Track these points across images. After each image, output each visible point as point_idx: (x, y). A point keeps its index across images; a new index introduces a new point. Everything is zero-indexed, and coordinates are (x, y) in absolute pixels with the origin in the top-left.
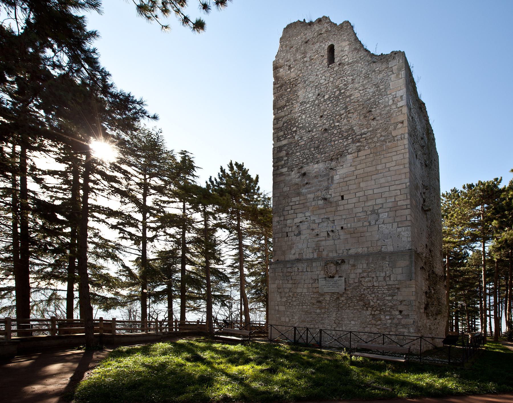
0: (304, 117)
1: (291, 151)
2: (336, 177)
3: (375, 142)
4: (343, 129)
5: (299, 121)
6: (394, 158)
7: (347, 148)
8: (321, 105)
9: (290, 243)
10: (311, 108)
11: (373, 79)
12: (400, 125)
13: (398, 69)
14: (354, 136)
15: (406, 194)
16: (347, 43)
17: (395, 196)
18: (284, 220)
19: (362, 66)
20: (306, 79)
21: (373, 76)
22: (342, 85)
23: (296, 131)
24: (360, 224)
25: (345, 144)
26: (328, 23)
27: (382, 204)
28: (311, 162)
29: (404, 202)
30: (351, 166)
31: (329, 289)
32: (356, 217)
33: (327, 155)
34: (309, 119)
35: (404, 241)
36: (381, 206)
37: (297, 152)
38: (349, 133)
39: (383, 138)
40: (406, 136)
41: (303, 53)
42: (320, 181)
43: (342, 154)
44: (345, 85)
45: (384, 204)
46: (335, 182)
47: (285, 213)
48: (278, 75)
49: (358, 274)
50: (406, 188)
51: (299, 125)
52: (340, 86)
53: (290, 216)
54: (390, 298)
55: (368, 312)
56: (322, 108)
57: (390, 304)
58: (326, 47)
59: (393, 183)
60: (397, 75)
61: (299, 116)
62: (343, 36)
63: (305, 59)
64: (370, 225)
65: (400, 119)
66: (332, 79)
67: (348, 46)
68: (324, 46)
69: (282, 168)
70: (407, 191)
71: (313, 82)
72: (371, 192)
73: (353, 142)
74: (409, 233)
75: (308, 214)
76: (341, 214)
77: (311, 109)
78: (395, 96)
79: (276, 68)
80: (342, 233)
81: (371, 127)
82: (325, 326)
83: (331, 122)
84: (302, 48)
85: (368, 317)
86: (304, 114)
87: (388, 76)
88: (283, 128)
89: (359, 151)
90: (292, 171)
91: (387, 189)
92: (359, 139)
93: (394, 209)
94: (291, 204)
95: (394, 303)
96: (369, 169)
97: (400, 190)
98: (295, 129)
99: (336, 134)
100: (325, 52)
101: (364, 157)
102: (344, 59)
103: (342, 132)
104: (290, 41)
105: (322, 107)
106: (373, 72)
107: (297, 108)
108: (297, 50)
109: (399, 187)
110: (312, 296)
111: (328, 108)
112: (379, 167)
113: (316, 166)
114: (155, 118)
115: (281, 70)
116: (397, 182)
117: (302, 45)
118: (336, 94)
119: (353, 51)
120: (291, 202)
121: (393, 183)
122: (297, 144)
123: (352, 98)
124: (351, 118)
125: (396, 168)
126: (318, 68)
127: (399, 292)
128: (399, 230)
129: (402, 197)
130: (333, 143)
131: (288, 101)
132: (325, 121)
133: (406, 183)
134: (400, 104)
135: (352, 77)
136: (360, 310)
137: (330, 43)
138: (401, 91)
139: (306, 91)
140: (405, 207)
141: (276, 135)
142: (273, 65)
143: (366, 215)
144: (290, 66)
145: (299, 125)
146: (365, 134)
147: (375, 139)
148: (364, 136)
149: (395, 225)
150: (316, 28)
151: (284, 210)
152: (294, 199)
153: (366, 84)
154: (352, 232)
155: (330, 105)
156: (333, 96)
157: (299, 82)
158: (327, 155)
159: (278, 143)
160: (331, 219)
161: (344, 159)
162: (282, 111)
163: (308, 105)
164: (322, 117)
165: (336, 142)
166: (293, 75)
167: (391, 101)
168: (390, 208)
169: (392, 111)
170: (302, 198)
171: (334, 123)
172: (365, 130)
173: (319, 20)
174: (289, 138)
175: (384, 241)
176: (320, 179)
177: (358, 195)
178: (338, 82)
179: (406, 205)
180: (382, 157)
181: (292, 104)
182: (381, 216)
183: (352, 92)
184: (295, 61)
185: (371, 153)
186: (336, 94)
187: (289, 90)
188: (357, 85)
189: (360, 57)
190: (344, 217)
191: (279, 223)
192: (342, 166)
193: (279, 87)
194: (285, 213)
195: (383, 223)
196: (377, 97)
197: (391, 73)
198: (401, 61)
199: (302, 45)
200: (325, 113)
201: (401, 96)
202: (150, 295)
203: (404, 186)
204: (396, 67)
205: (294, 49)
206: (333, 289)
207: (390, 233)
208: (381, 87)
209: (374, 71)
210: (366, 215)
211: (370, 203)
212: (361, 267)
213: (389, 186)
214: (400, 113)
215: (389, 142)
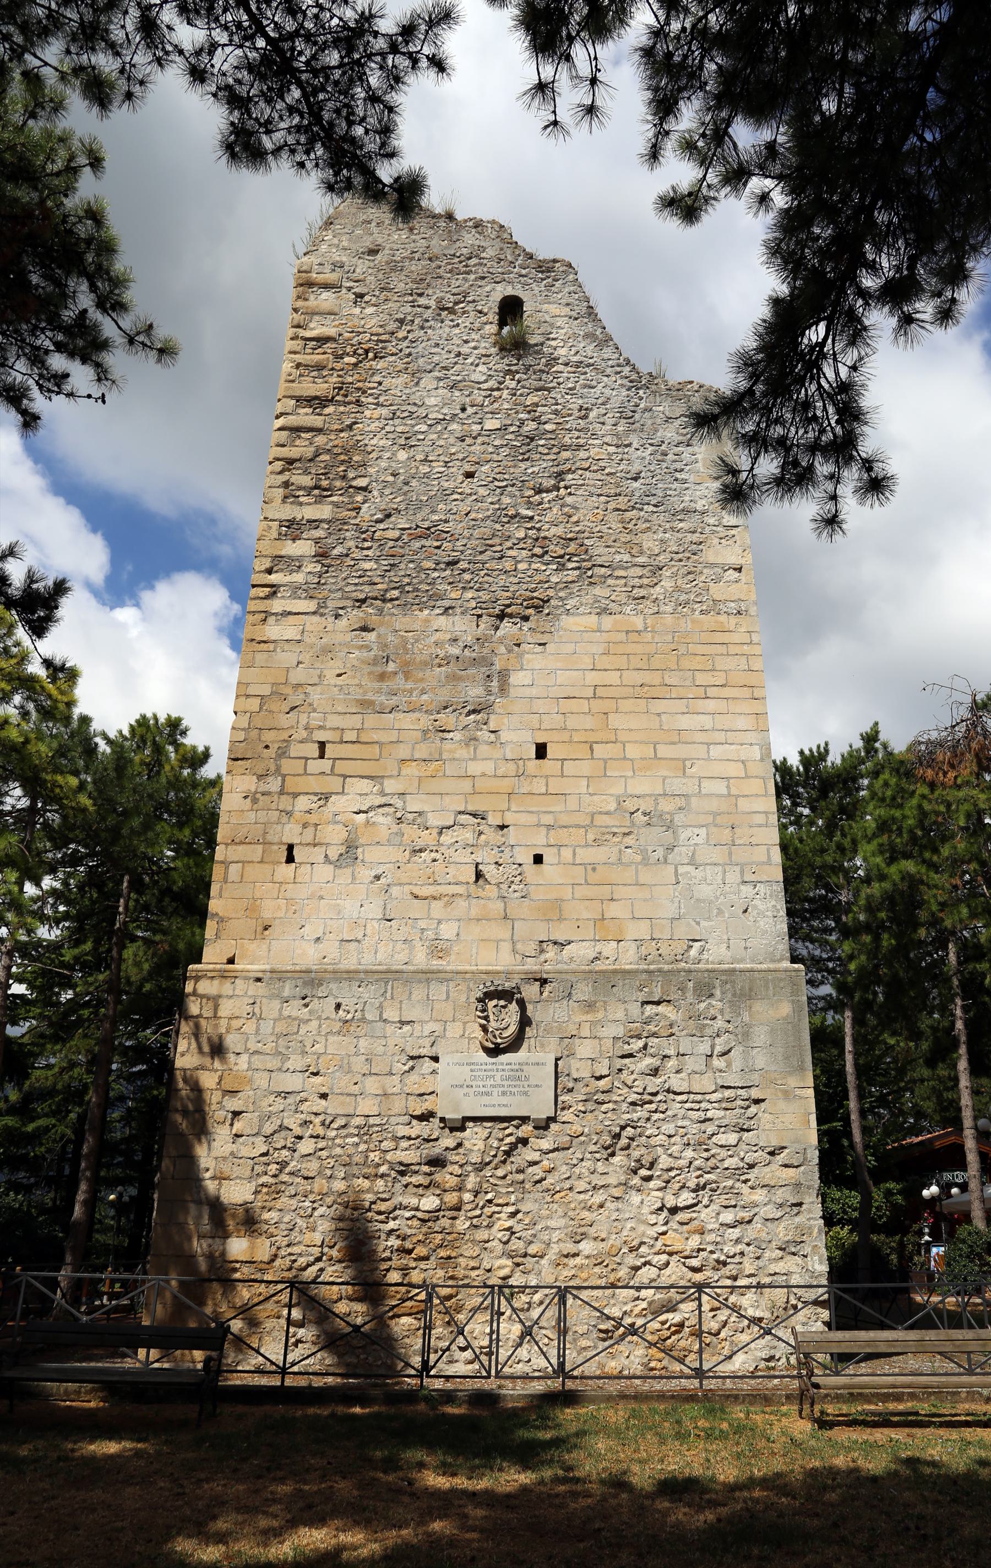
6: (721, 663)
18: (281, 793)
31: (486, 1100)
47: (287, 766)
54: (732, 1138)
57: (732, 1162)
59: (720, 737)
81: (642, 553)
82: (460, 1272)
114: (591, 110)
121: (720, 737)
149: (733, 876)
158: (484, 596)
159: (288, 506)
160: (494, 820)
168: (715, 814)
172: (626, 557)
175: (698, 923)
179: (766, 813)
181: (358, 403)
186: (526, 429)
191: (255, 801)
195: (692, 862)
202: (264, 838)
206: (504, 1100)
212: (620, 1015)
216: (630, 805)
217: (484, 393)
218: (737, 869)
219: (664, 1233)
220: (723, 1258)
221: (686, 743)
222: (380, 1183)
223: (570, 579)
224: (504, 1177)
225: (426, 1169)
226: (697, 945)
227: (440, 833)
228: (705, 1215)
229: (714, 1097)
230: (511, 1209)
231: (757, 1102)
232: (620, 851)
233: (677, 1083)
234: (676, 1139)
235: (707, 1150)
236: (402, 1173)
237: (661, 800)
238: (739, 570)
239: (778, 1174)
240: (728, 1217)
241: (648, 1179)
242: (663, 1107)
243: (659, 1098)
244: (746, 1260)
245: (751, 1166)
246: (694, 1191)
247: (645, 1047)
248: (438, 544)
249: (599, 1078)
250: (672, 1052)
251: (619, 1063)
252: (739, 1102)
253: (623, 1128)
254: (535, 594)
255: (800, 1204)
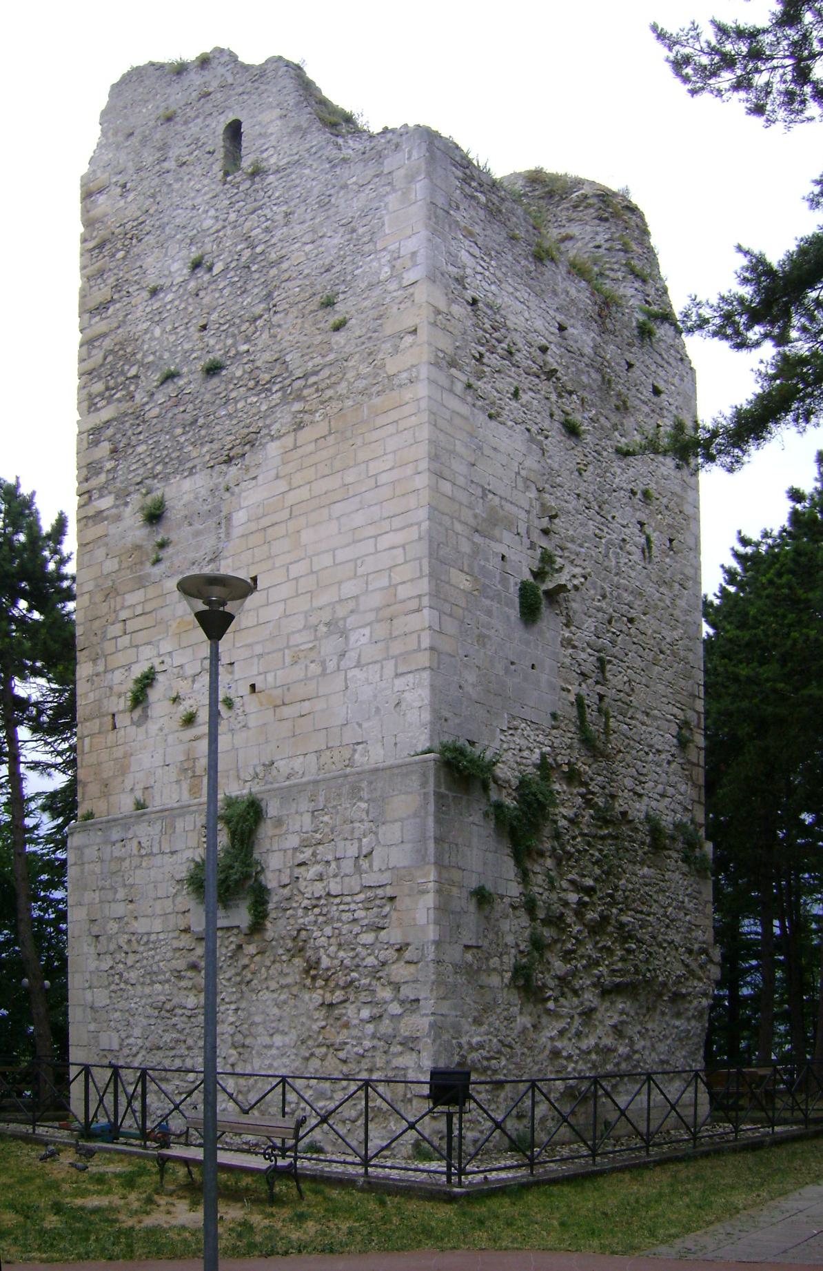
0: (157, 332)
1: (125, 441)
2: (240, 517)
3: (341, 398)
4: (258, 364)
5: (146, 347)
7: (268, 422)
8: (202, 294)
9: (119, 752)
10: (176, 303)
11: (340, 209)
12: (409, 339)
13: (406, 176)
14: (287, 382)
15: (419, 559)
16: (278, 112)
17: (390, 569)
19: (313, 175)
20: (166, 220)
21: (340, 200)
22: (259, 230)
23: (136, 377)
24: (297, 672)
25: (264, 408)
26: (225, 64)
27: (356, 597)
28: (175, 472)
29: (413, 585)
30: (277, 477)
32: (288, 647)
33: (216, 446)
34: (172, 338)
35: (411, 724)
36: (352, 604)
37: (140, 443)
38: (275, 373)
39: (361, 384)
40: (424, 372)
41: (160, 149)
42: (198, 534)
43: (251, 441)
44: (267, 230)
45: (362, 599)
46: (236, 532)
47: (109, 647)
48: (92, 214)
49: (290, 852)
50: (420, 538)
51: (144, 356)
52: (253, 233)
53: (121, 659)
55: (317, 996)
56: (204, 301)
57: (371, 961)
58: (221, 129)
60: (403, 193)
61: (146, 331)
62: (265, 95)
63: (166, 165)
64: (324, 673)
65: (409, 322)
66: (233, 217)
67: (278, 123)
68: (214, 125)
69: (101, 496)
70: (422, 549)
71: (184, 227)
72: (327, 560)
73: (284, 401)
74: (425, 693)
75: (166, 647)
76: (249, 641)
77: (177, 307)
78: (396, 255)
79: (89, 194)
80: (251, 704)
81: (331, 350)
83: (229, 342)
84: (158, 136)
85: (316, 1015)
86: (158, 323)
87: (381, 197)
88: (109, 371)
89: (300, 426)
90: (126, 504)
91: (368, 546)
92: (301, 390)
93: (386, 613)
94: (124, 615)
95: (383, 955)
96: (322, 486)
97: (403, 546)
98: (133, 372)
99: (240, 378)
100: (217, 141)
101: (311, 447)
102: (267, 160)
103: (257, 372)
104: (126, 118)
105: (206, 300)
106: (342, 188)
107: (141, 308)
108: (144, 141)
109: (398, 538)
110: (176, 944)
111: (221, 301)
112: (350, 477)
113: (187, 484)
115: (101, 199)
116: (397, 523)
117: (156, 127)
118: (243, 259)
119: (290, 134)
120: (123, 608)
121: (385, 525)
122: (139, 416)
123: (284, 266)
124: (279, 326)
125: (395, 475)
126: (198, 187)
127: (394, 915)
128: (399, 683)
129: (407, 571)
130: (231, 408)
131: (117, 287)
132: (212, 342)
133: (419, 524)
134: (409, 277)
135: (284, 208)
136: (295, 990)
137: (231, 117)
138: (414, 239)
139: (166, 255)
140: (414, 604)
141: (85, 391)
142: (82, 186)
143: (316, 639)
144: (124, 186)
145: (144, 356)
146: (316, 373)
147: (342, 388)
148: (313, 379)
150: (195, 79)
151: (104, 638)
152: (131, 599)
153: (321, 224)
154: (279, 702)
155: (226, 292)
156: (233, 265)
157: (148, 228)
158: (216, 446)
161: (260, 457)
162: (102, 319)
163: (170, 297)
164: (204, 328)
165: (240, 405)
166: (133, 211)
167: (387, 269)
168: (378, 610)
169: (388, 300)
170: (151, 592)
171: (234, 345)
173: (204, 62)
174: (119, 400)
175: (360, 725)
176: (198, 526)
177: (295, 570)
178: (248, 224)
179: (419, 596)
180: (359, 441)
182: (352, 638)
183: (283, 252)
184: (139, 170)
185: (330, 434)
186: (243, 259)
187: (121, 254)
188: (298, 230)
189: (308, 150)
190: (258, 649)
192: (255, 478)
193: (94, 248)
194: (109, 647)
195: (359, 665)
196: (348, 259)
197: (388, 188)
198: (415, 155)
199: (156, 127)
200: (214, 316)
201: (414, 254)
203: (413, 533)
204: (402, 172)
205: (135, 140)
207: (375, 696)
208: (361, 231)
209: (345, 187)
210: (316, 639)
211: (323, 599)
213: (375, 537)
214: (409, 304)
215: (378, 394)
216: (313, 620)
217: (212, 238)
218: (392, 662)
219: (323, 1028)
220: (361, 1051)
221: (360, 541)
222: (167, 986)
223: (273, 403)
224: (230, 979)
225: (189, 974)
226: (361, 746)
227: (193, 681)
228: (350, 1010)
229: (362, 897)
230: (233, 1007)
231: (392, 899)
232: (306, 667)
233: (335, 888)
234: (333, 940)
235: (354, 949)
236: (180, 978)
237: (338, 607)
238: (414, 332)
239: (401, 971)
240: (365, 1013)
241: (314, 978)
242: (325, 910)
243: (323, 901)
244: (378, 1053)
245: (384, 964)
246: (344, 988)
247: (314, 854)
248: (182, 409)
249: (285, 886)
250: (330, 858)
251: (297, 871)
252: (378, 902)
253: (299, 931)
254: (251, 429)
255: (417, 1000)
